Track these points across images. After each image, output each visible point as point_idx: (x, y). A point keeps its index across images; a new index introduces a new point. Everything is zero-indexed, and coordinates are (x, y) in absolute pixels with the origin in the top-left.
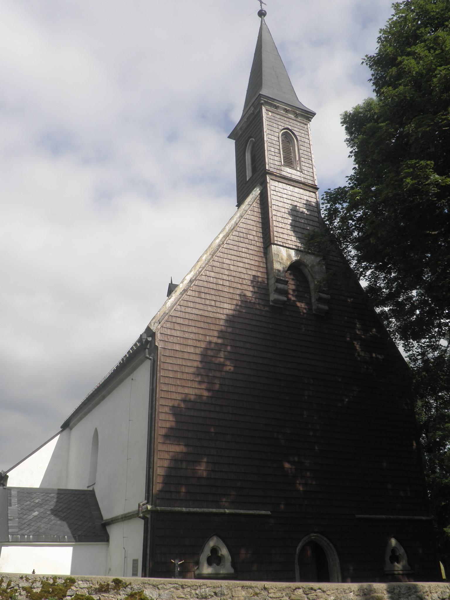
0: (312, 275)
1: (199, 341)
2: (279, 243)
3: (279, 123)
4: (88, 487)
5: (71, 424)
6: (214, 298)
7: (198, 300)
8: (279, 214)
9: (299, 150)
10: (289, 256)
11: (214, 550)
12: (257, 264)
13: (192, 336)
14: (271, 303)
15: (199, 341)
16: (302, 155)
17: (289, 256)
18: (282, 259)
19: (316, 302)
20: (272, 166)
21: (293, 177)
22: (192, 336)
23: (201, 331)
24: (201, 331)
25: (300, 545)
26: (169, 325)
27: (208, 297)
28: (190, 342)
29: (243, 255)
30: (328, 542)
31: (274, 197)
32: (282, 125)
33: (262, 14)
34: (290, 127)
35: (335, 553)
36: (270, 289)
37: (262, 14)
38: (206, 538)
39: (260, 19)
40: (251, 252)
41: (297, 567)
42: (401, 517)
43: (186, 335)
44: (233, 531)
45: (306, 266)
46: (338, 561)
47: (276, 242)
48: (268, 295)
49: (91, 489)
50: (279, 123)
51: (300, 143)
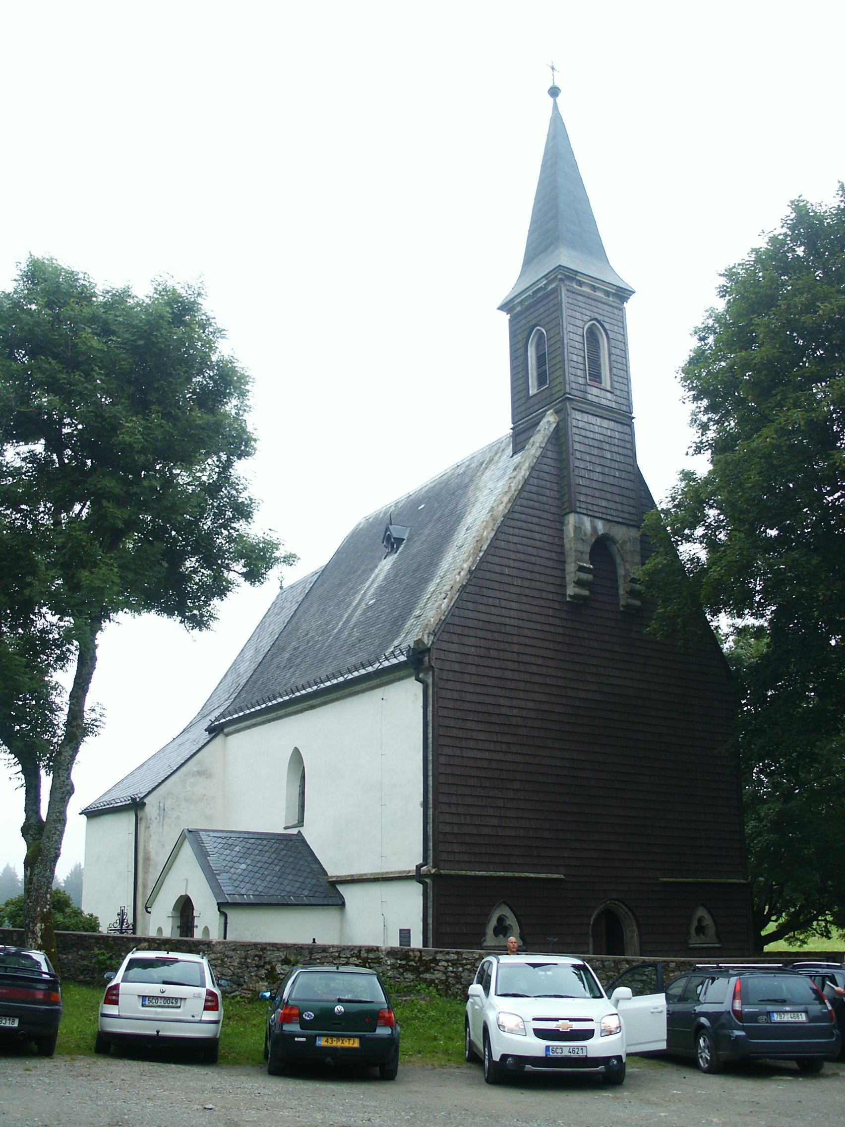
0: (622, 556)
1: (481, 657)
2: (582, 511)
3: (585, 311)
4: (285, 828)
5: (226, 730)
6: (498, 594)
7: (478, 599)
8: (582, 465)
9: (610, 355)
10: (594, 528)
11: (501, 920)
12: (550, 540)
13: (473, 650)
14: (568, 599)
15: (481, 657)
16: (615, 364)
17: (594, 528)
18: (585, 535)
19: (626, 595)
20: (574, 386)
21: (604, 402)
22: (473, 650)
23: (483, 643)
24: (483, 643)
25: (596, 913)
26: (445, 636)
27: (491, 593)
28: (470, 659)
29: (534, 527)
30: (627, 910)
31: (576, 438)
32: (588, 313)
33: (554, 92)
34: (599, 318)
35: (634, 923)
36: (568, 578)
37: (554, 92)
38: (492, 906)
39: (552, 100)
40: (543, 522)
41: (591, 939)
42: (712, 880)
43: (466, 650)
44: (515, 893)
45: (614, 542)
46: (636, 934)
47: (578, 510)
48: (564, 586)
49: (294, 831)
50: (585, 311)
51: (613, 343)
